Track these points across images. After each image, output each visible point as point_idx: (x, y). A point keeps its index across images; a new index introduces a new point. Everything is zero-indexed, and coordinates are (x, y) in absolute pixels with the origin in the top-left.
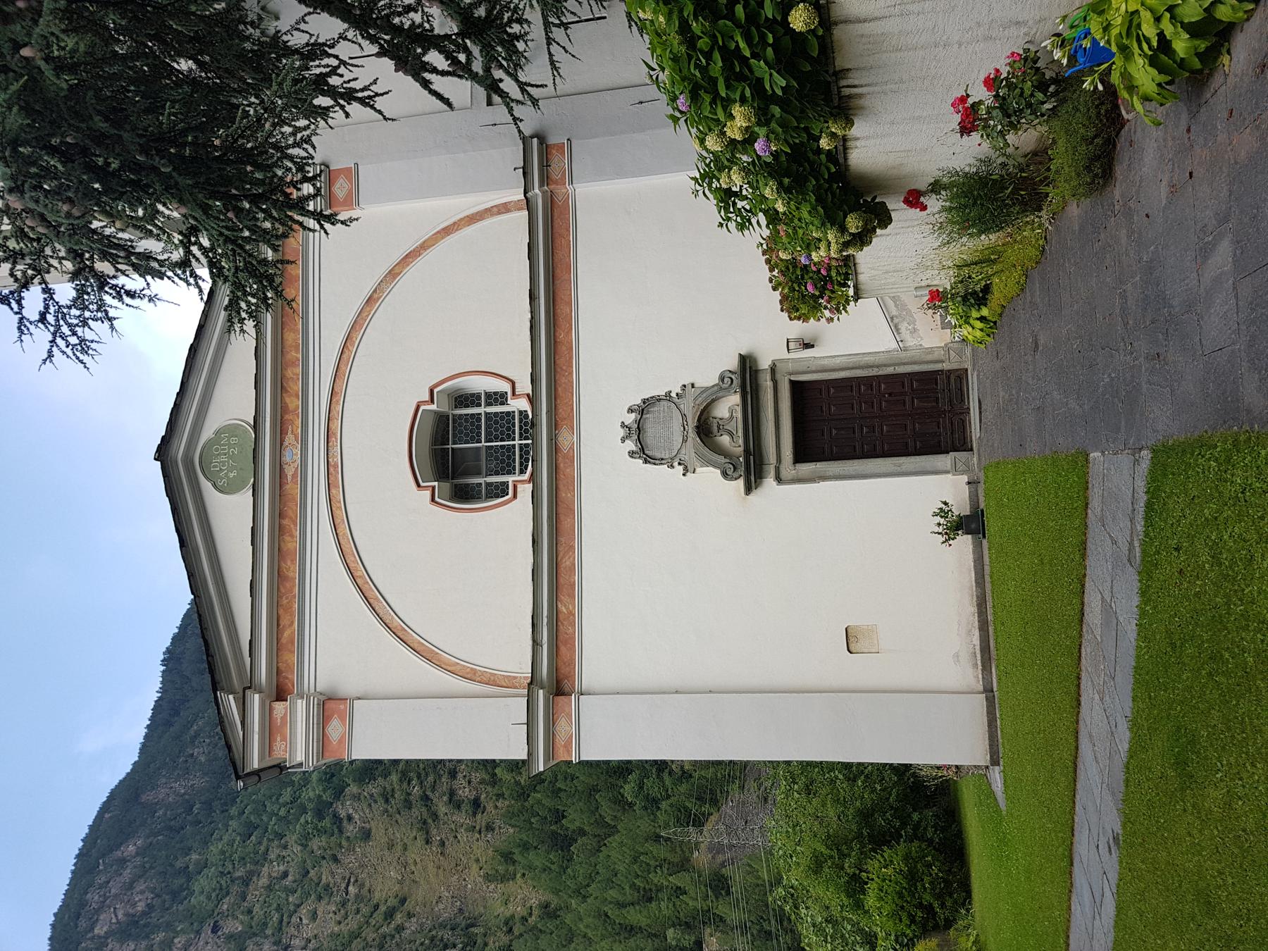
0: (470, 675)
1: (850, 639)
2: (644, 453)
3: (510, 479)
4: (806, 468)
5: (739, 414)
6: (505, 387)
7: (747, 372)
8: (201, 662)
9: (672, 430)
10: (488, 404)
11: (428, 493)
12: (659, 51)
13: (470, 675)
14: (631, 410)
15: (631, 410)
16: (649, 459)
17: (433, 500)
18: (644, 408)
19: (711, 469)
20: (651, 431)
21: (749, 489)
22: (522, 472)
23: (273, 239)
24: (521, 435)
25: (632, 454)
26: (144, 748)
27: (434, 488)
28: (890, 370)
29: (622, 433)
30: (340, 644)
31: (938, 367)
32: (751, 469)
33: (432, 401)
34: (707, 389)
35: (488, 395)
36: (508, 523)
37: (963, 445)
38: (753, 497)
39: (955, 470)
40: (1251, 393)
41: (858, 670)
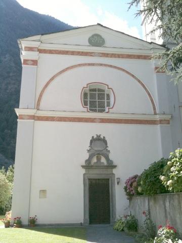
0: (41, 96)
1: (43, 192)
2: (93, 141)
3: (88, 107)
4: (87, 182)
5: (102, 165)
6: (111, 106)
7: (111, 166)
8: (49, 26)
9: (98, 147)
10: (107, 102)
11: (86, 86)
12: (166, 18)
13: (41, 96)
14: (104, 137)
15: (104, 137)
16: (91, 142)
17: (84, 87)
18: (104, 141)
19: (88, 157)
20: (98, 143)
21: (83, 167)
22: (90, 110)
23: (146, 194)
24: (100, 101)
25: (93, 137)
26: (26, 10)
27: (87, 88)
28: (111, 204)
29: (99, 135)
30: (50, 64)
31: (111, 217)
32: (88, 166)
33: (108, 88)
34: (108, 157)
35: (109, 102)
36: (77, 107)
37: (91, 222)
38: (81, 168)
39: (85, 219)
40: (142, 5)
41: (35, 193)
